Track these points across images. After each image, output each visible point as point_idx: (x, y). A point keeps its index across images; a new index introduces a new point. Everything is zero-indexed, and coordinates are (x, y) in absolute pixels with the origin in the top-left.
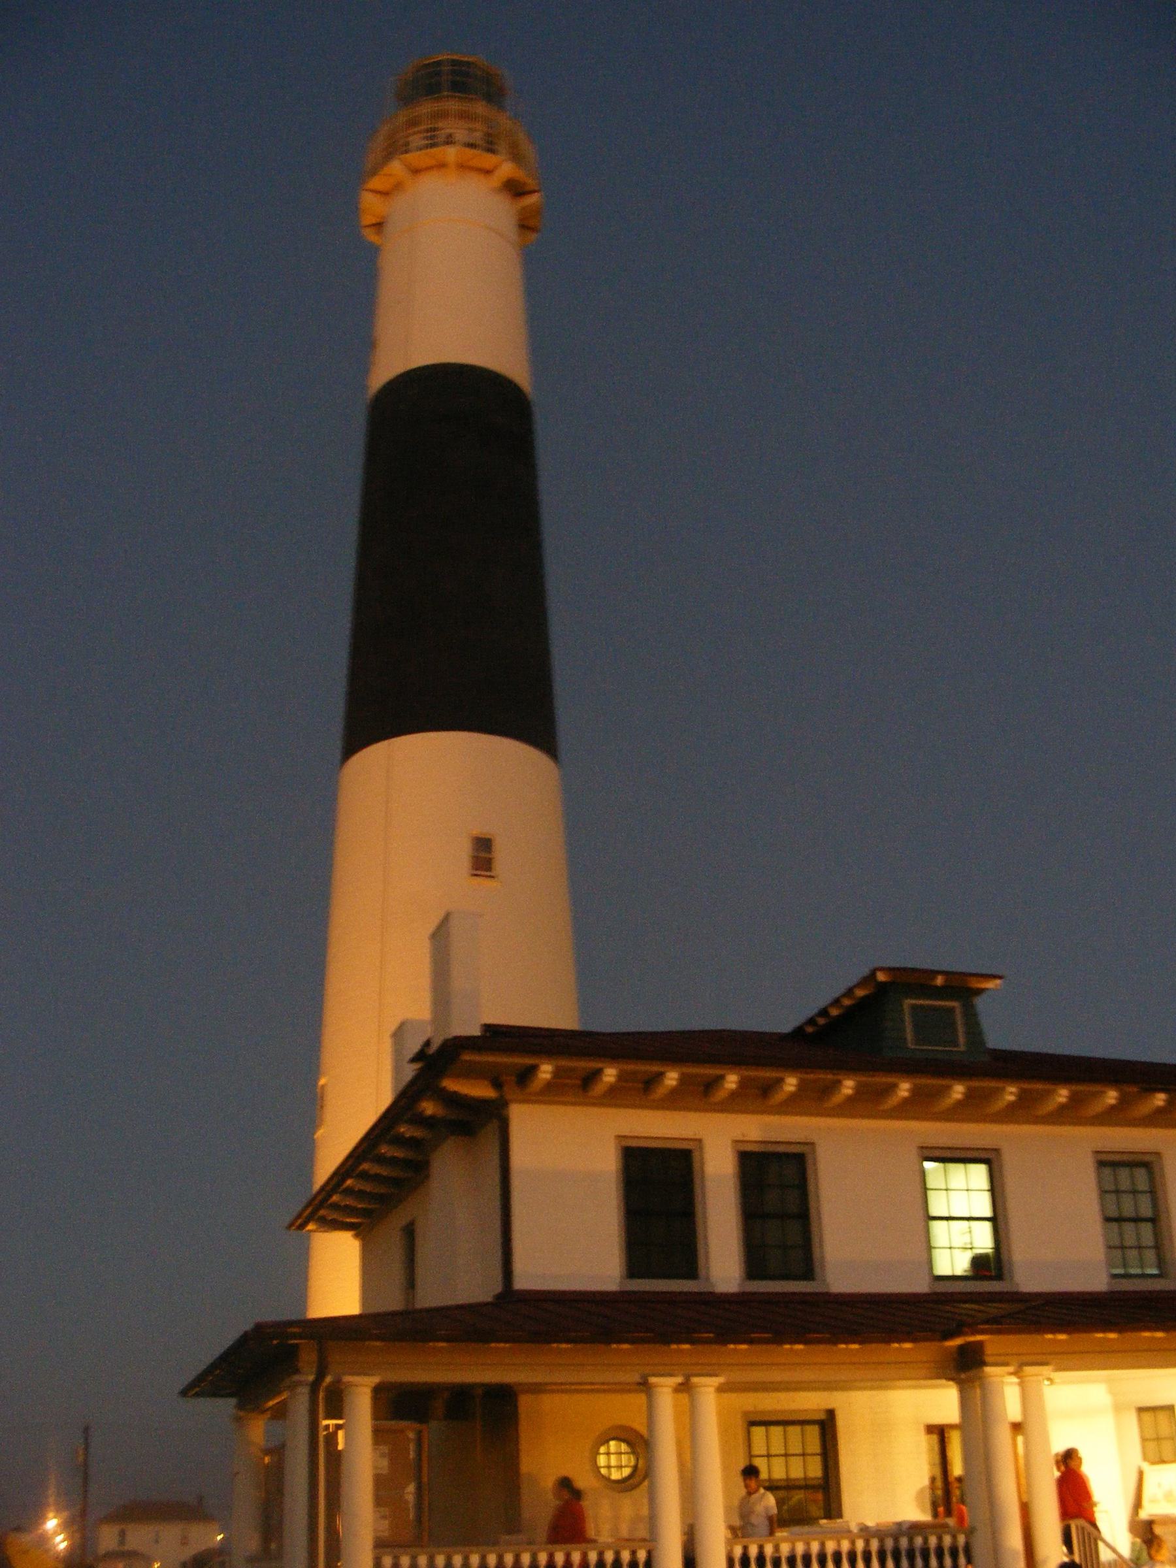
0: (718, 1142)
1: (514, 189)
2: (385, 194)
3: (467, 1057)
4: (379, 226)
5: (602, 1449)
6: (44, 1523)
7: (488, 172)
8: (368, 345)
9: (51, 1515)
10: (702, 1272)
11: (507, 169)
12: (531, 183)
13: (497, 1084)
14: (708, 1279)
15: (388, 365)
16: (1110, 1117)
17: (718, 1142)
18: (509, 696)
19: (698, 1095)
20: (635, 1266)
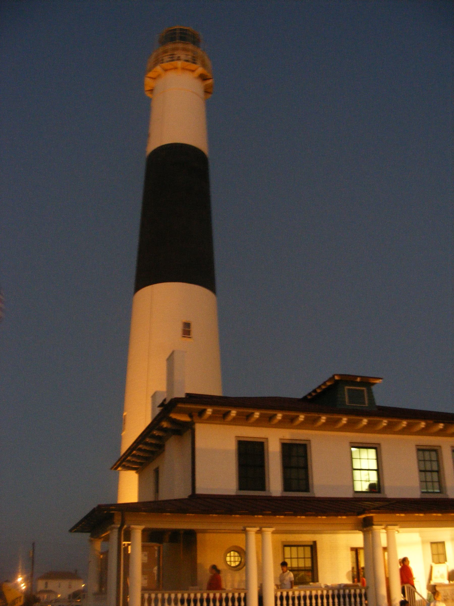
0: (274, 439)
1: (203, 78)
2: (154, 79)
3: (180, 405)
4: (152, 91)
5: (228, 555)
6: (17, 579)
7: (193, 71)
8: (145, 136)
9: (20, 576)
10: (267, 488)
11: (200, 70)
12: (209, 75)
13: (191, 416)
14: (269, 491)
15: (154, 143)
16: (422, 432)
17: (274, 439)
18: (197, 269)
19: (267, 421)
20: (241, 487)
